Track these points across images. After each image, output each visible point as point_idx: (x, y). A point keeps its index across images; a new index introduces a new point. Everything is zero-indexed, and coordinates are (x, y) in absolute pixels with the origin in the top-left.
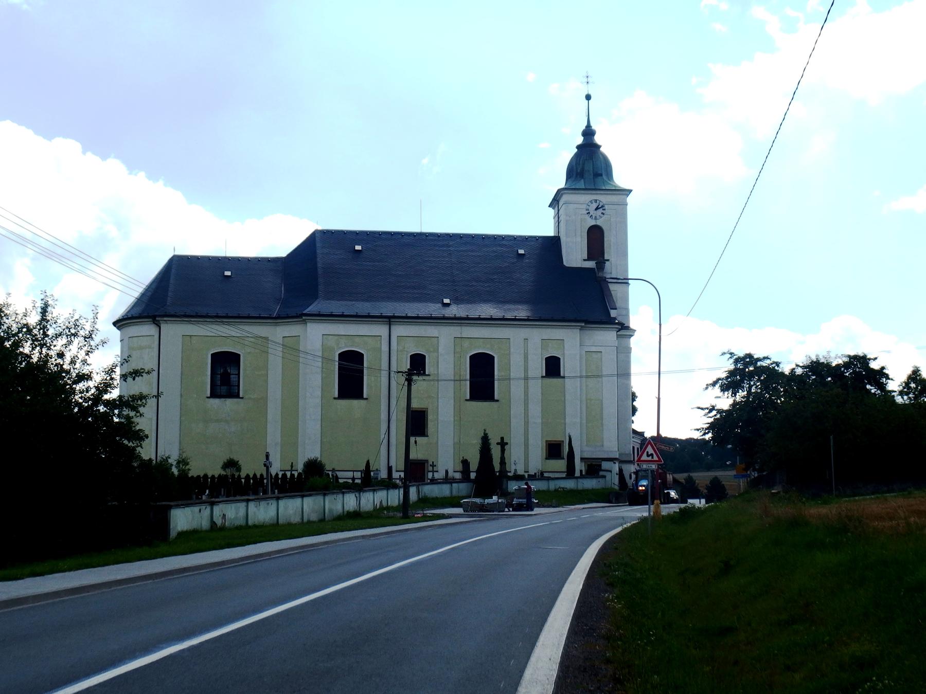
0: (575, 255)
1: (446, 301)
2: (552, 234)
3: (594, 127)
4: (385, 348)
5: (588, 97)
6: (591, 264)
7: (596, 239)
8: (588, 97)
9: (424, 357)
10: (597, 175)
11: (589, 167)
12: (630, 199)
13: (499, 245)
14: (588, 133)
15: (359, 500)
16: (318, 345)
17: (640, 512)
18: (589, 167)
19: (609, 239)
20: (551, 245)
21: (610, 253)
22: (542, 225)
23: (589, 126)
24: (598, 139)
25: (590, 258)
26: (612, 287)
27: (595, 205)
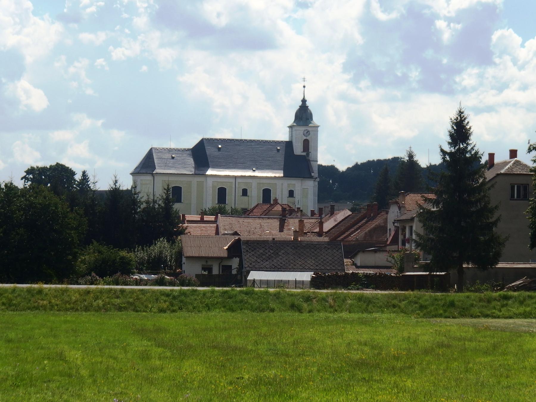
0: (298, 150)
1: (254, 169)
2: (288, 140)
3: (306, 98)
4: (234, 186)
5: (304, 87)
6: (304, 154)
7: (306, 145)
8: (304, 87)
9: (247, 190)
10: (307, 119)
11: (303, 115)
12: (319, 129)
13: (271, 145)
14: (304, 101)
15: (335, 221)
16: (211, 185)
17: (302, 290)
18: (303, 115)
19: (311, 144)
20: (289, 145)
21: (311, 150)
22: (283, 136)
23: (304, 98)
24: (308, 104)
25: (304, 151)
26: (312, 163)
27: (306, 132)
